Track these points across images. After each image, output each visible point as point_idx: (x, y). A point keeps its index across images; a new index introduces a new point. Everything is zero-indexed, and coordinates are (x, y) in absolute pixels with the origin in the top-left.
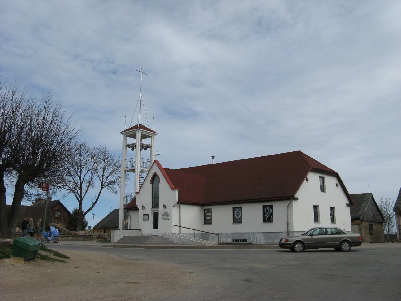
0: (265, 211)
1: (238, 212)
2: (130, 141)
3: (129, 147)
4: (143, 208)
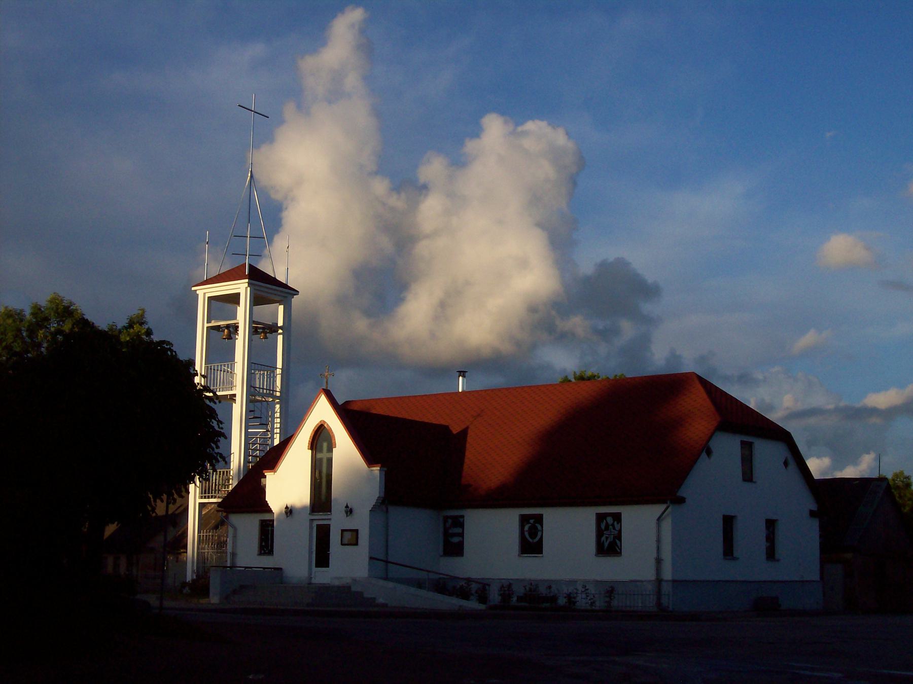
0: (603, 526)
4: (346, 512)
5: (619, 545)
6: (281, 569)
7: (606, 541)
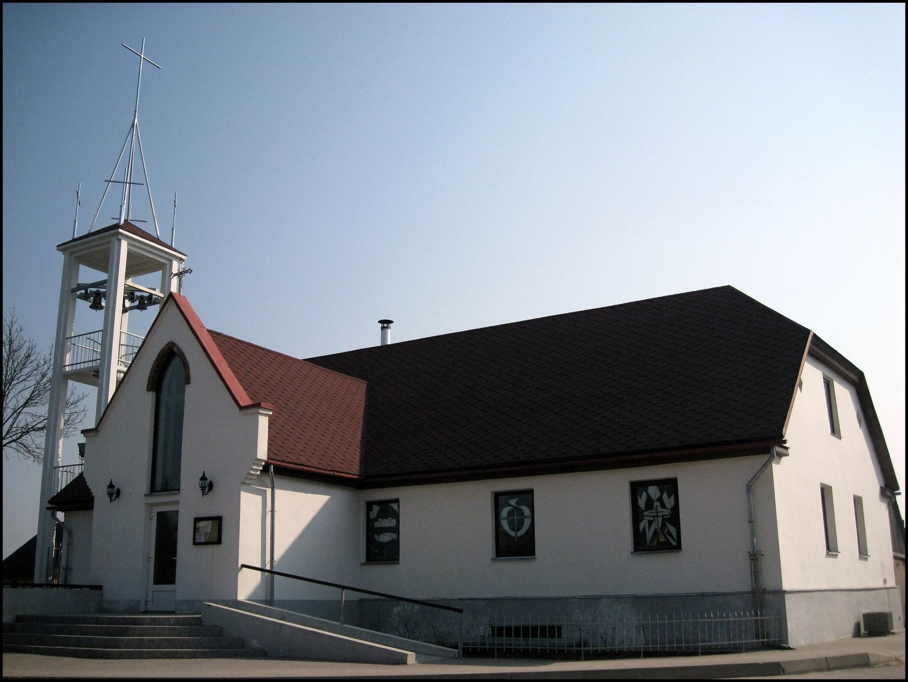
0: (642, 502)
1: (517, 511)
2: (88, 275)
3: (85, 297)
5: (674, 533)
6: (99, 588)
7: (649, 529)
